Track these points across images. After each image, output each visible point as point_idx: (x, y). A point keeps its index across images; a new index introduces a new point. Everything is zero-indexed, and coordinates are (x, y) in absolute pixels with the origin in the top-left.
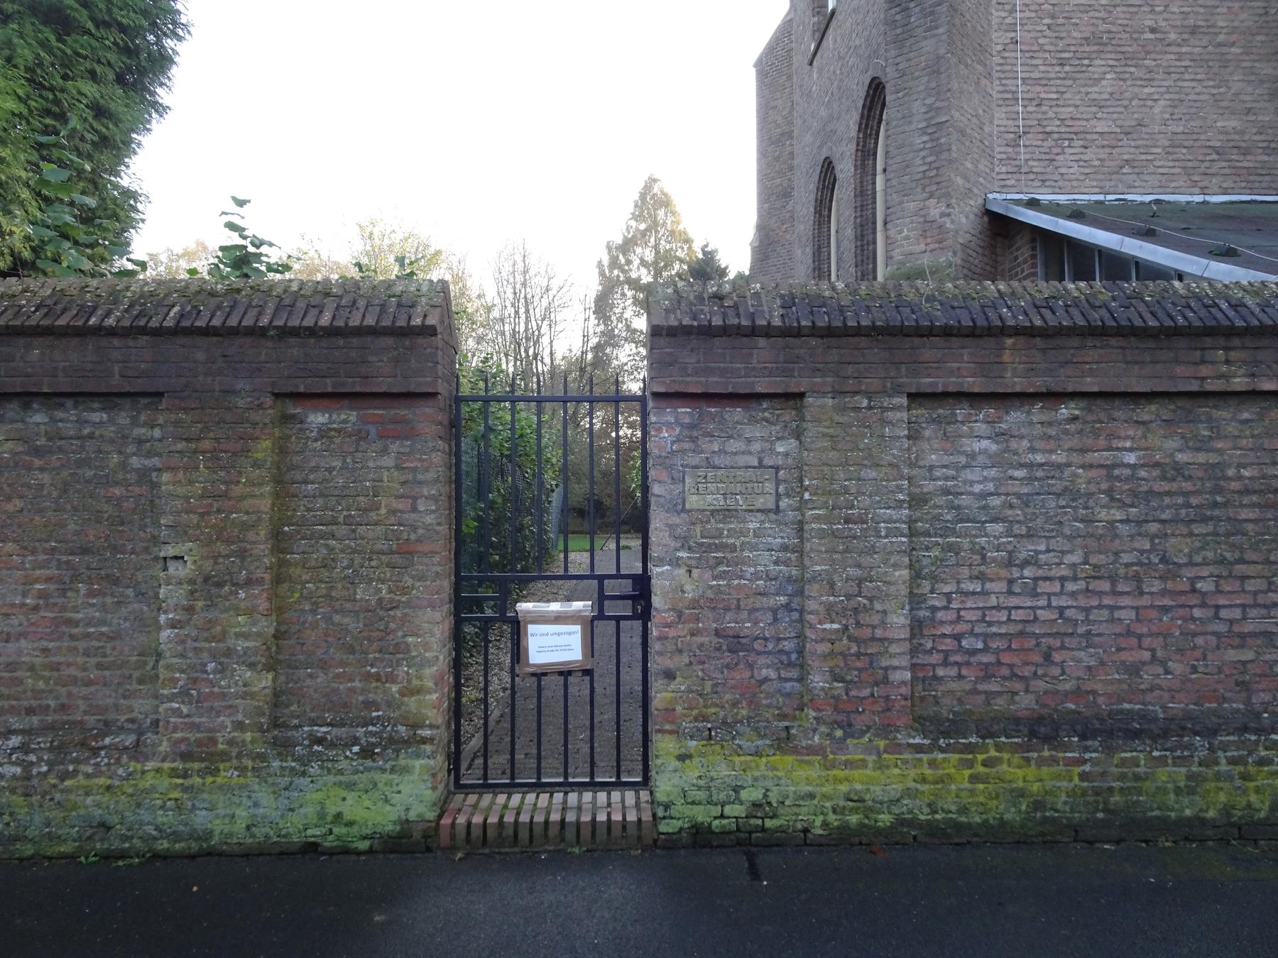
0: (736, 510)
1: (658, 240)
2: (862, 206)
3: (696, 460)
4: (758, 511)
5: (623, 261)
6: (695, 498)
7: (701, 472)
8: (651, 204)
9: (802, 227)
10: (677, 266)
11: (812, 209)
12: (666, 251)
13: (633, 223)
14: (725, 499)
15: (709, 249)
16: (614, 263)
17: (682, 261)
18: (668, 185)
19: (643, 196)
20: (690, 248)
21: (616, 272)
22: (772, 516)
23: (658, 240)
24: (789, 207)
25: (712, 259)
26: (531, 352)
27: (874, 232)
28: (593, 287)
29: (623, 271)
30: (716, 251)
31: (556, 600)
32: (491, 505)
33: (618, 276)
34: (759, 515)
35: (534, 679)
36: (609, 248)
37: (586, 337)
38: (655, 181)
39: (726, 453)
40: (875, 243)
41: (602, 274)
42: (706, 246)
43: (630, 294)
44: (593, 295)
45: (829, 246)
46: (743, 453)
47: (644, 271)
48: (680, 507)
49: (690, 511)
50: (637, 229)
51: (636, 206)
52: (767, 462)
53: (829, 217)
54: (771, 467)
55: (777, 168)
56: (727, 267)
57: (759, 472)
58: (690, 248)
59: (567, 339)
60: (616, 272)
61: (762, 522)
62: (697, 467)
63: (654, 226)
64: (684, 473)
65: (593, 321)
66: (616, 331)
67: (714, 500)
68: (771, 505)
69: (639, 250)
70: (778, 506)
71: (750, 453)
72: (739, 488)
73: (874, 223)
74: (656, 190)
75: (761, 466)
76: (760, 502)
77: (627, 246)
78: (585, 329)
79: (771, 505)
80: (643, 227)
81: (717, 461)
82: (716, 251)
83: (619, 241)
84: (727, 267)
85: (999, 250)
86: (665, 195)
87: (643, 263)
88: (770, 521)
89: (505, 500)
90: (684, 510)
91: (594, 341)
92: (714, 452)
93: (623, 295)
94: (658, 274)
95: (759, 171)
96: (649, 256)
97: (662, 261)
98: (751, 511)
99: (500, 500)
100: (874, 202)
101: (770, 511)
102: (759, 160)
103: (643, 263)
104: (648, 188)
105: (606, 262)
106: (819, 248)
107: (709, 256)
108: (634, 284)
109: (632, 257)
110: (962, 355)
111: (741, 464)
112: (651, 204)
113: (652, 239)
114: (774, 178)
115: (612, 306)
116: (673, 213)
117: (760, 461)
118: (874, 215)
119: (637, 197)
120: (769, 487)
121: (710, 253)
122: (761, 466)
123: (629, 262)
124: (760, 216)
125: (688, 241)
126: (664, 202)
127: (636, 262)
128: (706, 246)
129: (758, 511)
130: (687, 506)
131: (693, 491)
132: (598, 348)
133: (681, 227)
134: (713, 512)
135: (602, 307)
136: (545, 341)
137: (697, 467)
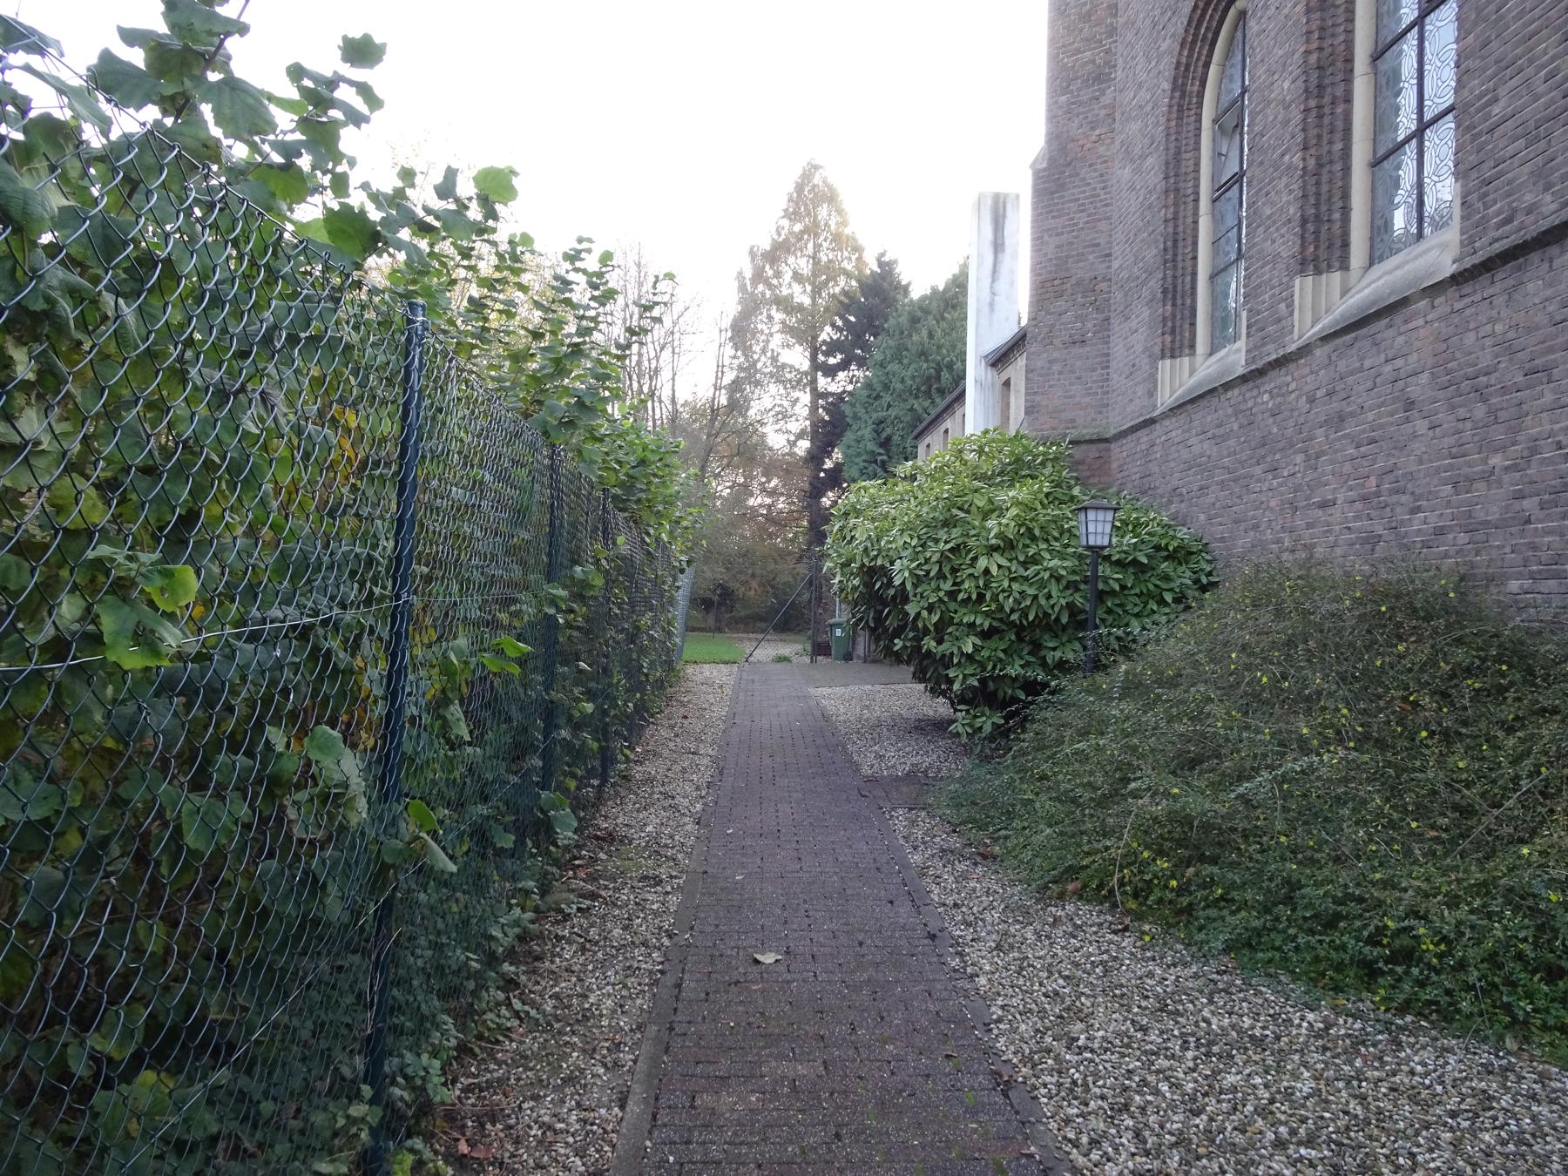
1: (817, 247)
2: (1322, 29)
5: (770, 273)
8: (810, 199)
9: (1134, 127)
10: (842, 281)
11: (1166, 86)
12: (830, 261)
13: (785, 223)
15: (886, 259)
16: (758, 276)
17: (848, 275)
18: (834, 174)
19: (799, 188)
20: (859, 259)
21: (761, 287)
23: (817, 247)
24: (1106, 100)
25: (891, 272)
26: (646, 389)
27: (1348, 79)
28: (732, 308)
29: (770, 286)
30: (896, 262)
32: (580, 592)
33: (763, 294)
36: (752, 254)
37: (720, 369)
38: (816, 167)
40: (1348, 100)
41: (742, 288)
42: (883, 255)
43: (778, 316)
44: (727, 322)
45: (1197, 148)
47: (797, 288)
50: (791, 233)
51: (790, 200)
53: (1201, 95)
55: (1086, 33)
56: (909, 284)
58: (859, 259)
59: (689, 374)
60: (761, 287)
63: (813, 230)
65: (729, 350)
66: (759, 365)
69: (791, 260)
73: (1349, 60)
74: (817, 180)
77: (776, 254)
78: (720, 356)
80: (798, 227)
82: (896, 262)
83: (766, 245)
84: (909, 284)
86: (830, 188)
87: (797, 277)
89: (610, 582)
91: (729, 377)
93: (770, 317)
94: (816, 292)
95: (1053, 40)
96: (805, 266)
97: (822, 274)
99: (599, 581)
100: (1351, 20)
102: (1053, 24)
103: (797, 277)
104: (807, 176)
105: (748, 274)
106: (1178, 153)
107: (887, 268)
108: (786, 304)
109: (783, 268)
112: (810, 199)
113: (810, 245)
114: (1078, 51)
115: (754, 333)
116: (840, 212)
118: (1349, 44)
119: (791, 188)
121: (888, 264)
123: (778, 275)
124: (1052, 117)
125: (857, 249)
126: (830, 197)
127: (788, 276)
128: (883, 255)
132: (736, 386)
133: (848, 231)
135: (741, 333)
136: (665, 375)
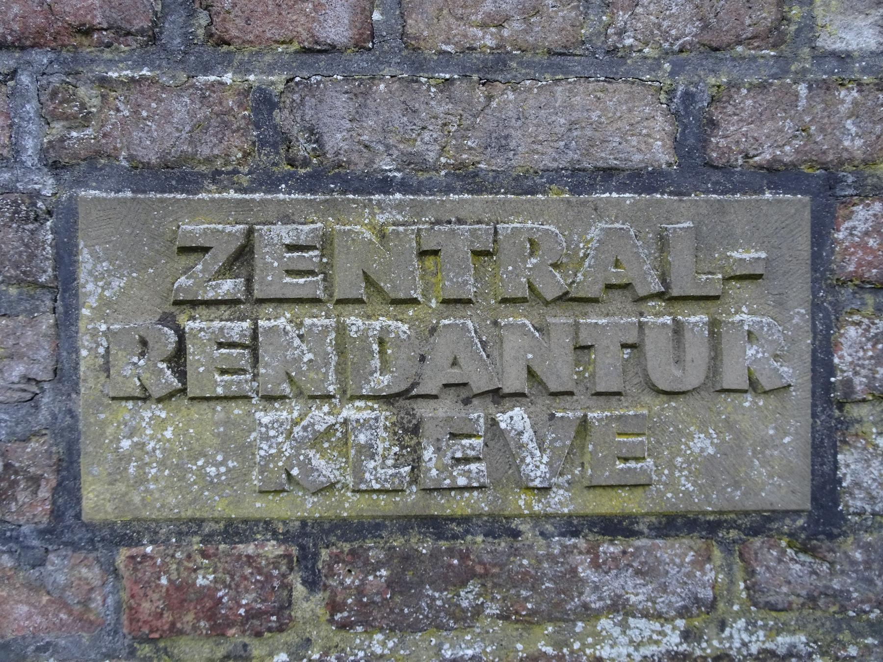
0: (500, 527)
3: (165, 118)
4: (671, 525)
6: (158, 429)
7: (210, 218)
14: (410, 432)
22: (788, 569)
31: (381, 363)
34: (676, 553)
35: (797, 205)
39: (415, 59)
46: (559, 59)
48: (31, 507)
49: (119, 535)
52: (752, 131)
54: (777, 175)
57: (683, 213)
61: (703, 612)
62: (174, 174)
64: (67, 219)
67: (301, 440)
68: (776, 480)
70: (826, 488)
71: (612, 62)
72: (521, 340)
75: (697, 164)
76: (690, 458)
79: (776, 480)
81: (339, 123)
85: (645, 392)
88: (760, 602)
90: (65, 525)
92: (317, 51)
98: (615, 527)
101: (762, 524)
110: (361, 215)
111: (530, 151)
117: (694, 125)
120: (766, 337)
122: (697, 164)
129: (671, 525)
130: (97, 500)
131: (131, 370)
134: (307, 543)
137: (174, 174)
